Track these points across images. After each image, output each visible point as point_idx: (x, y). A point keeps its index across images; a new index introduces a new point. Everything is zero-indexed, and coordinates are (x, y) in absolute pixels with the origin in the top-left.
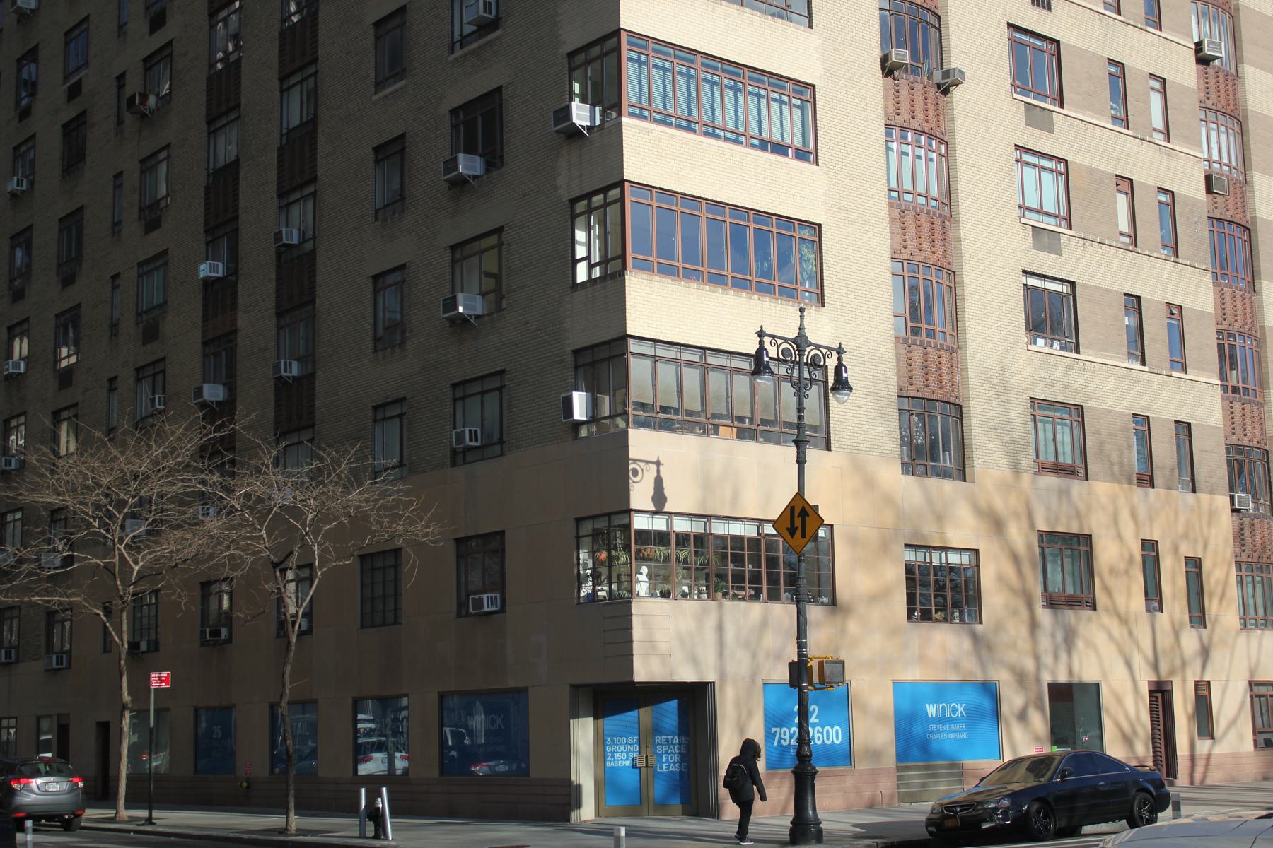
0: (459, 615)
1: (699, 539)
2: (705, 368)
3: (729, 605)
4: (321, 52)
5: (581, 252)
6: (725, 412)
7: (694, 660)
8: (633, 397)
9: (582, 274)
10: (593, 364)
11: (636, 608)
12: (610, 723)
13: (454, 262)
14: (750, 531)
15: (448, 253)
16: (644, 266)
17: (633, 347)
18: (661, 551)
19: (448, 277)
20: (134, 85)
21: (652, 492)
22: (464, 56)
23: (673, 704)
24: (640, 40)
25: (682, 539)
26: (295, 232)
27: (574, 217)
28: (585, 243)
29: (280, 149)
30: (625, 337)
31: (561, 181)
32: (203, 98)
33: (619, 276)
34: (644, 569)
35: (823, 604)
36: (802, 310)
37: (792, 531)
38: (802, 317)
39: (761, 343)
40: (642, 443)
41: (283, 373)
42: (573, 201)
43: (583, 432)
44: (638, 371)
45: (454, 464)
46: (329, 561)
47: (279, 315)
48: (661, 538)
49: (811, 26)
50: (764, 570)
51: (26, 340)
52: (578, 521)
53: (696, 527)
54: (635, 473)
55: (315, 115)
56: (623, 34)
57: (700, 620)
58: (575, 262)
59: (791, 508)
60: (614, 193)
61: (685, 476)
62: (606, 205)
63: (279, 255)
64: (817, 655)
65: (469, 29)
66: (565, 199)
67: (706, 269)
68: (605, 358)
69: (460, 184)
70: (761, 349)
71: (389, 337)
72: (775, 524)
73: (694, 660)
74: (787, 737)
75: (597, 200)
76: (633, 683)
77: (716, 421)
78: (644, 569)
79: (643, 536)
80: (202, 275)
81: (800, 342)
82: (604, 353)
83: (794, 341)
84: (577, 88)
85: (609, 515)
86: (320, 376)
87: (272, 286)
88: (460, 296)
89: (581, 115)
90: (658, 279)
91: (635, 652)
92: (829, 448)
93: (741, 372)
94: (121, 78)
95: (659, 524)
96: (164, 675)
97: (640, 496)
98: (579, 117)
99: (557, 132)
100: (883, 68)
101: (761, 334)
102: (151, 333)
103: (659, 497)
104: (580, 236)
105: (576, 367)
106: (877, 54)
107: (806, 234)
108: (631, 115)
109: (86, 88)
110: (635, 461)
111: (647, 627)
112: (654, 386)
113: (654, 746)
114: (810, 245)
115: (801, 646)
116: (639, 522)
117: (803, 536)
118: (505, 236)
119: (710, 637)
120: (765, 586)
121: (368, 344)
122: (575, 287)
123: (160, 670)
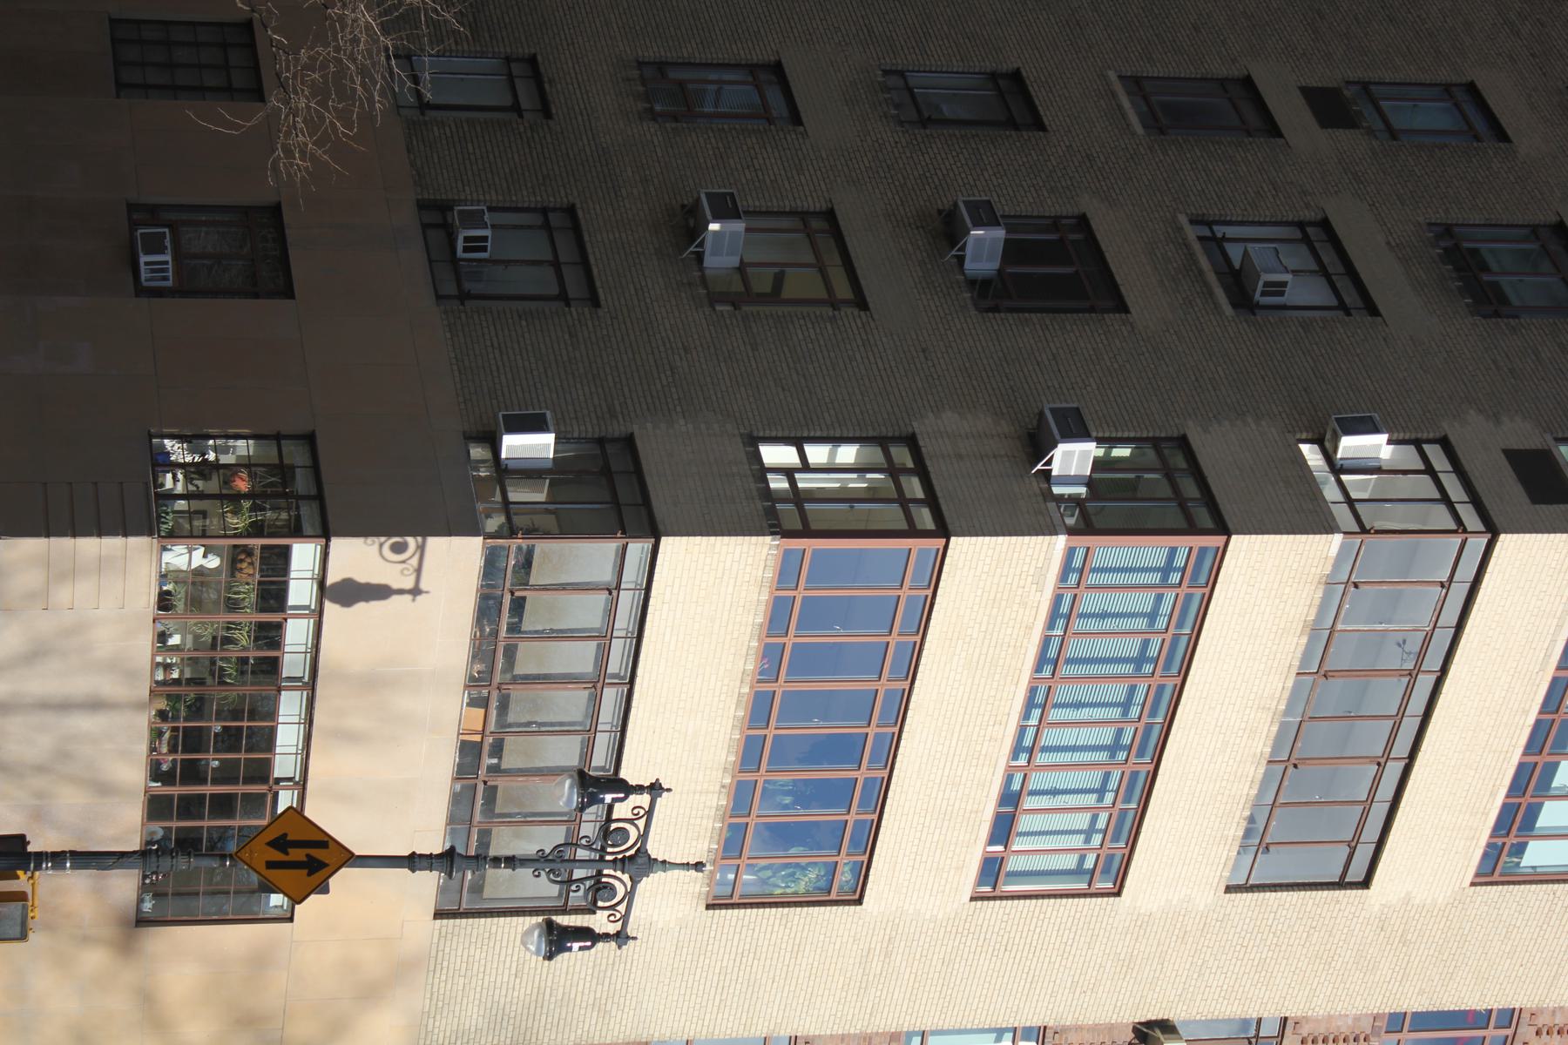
0: (132, 207)
1: (271, 667)
2: (596, 682)
3: (142, 722)
5: (817, 454)
9: (776, 455)
11: (139, 544)
13: (803, 215)
14: (284, 765)
15: (815, 204)
16: (787, 572)
17: (638, 549)
18: (247, 590)
21: (362, 578)
22: (1187, 246)
24: (1209, 573)
25: (270, 635)
27: (883, 442)
28: (834, 461)
34: (213, 562)
35: (140, 901)
36: (698, 866)
37: (281, 843)
38: (686, 866)
39: (639, 789)
40: (455, 563)
42: (911, 442)
43: (478, 452)
44: (592, 557)
48: (274, 595)
49: (1229, 889)
50: (208, 789)
52: (310, 439)
53: (293, 662)
54: (399, 549)
57: (116, 666)
58: (798, 443)
59: (324, 841)
60: (925, 518)
61: (391, 646)
62: (904, 502)
66: (917, 427)
69: (949, 231)
70: (628, 789)
72: (297, 812)
75: (914, 487)
77: (494, 704)
79: (279, 561)
81: (640, 863)
82: (626, 492)
84: (1122, 452)
85: (319, 497)
89: (1072, 459)
90: (765, 597)
91: (53, 539)
92: (439, 915)
95: (300, 592)
97: (355, 557)
98: (1067, 454)
99: (1041, 414)
100: (1150, 1024)
101: (655, 789)
103: (352, 593)
104: (848, 454)
105: (601, 442)
106: (1175, 1014)
107: (844, 876)
108: (1070, 553)
110: (421, 549)
111: (101, 565)
112: (563, 587)
115: (57, 858)
116: (303, 555)
117: (271, 865)
119: (82, 685)
120: (176, 790)
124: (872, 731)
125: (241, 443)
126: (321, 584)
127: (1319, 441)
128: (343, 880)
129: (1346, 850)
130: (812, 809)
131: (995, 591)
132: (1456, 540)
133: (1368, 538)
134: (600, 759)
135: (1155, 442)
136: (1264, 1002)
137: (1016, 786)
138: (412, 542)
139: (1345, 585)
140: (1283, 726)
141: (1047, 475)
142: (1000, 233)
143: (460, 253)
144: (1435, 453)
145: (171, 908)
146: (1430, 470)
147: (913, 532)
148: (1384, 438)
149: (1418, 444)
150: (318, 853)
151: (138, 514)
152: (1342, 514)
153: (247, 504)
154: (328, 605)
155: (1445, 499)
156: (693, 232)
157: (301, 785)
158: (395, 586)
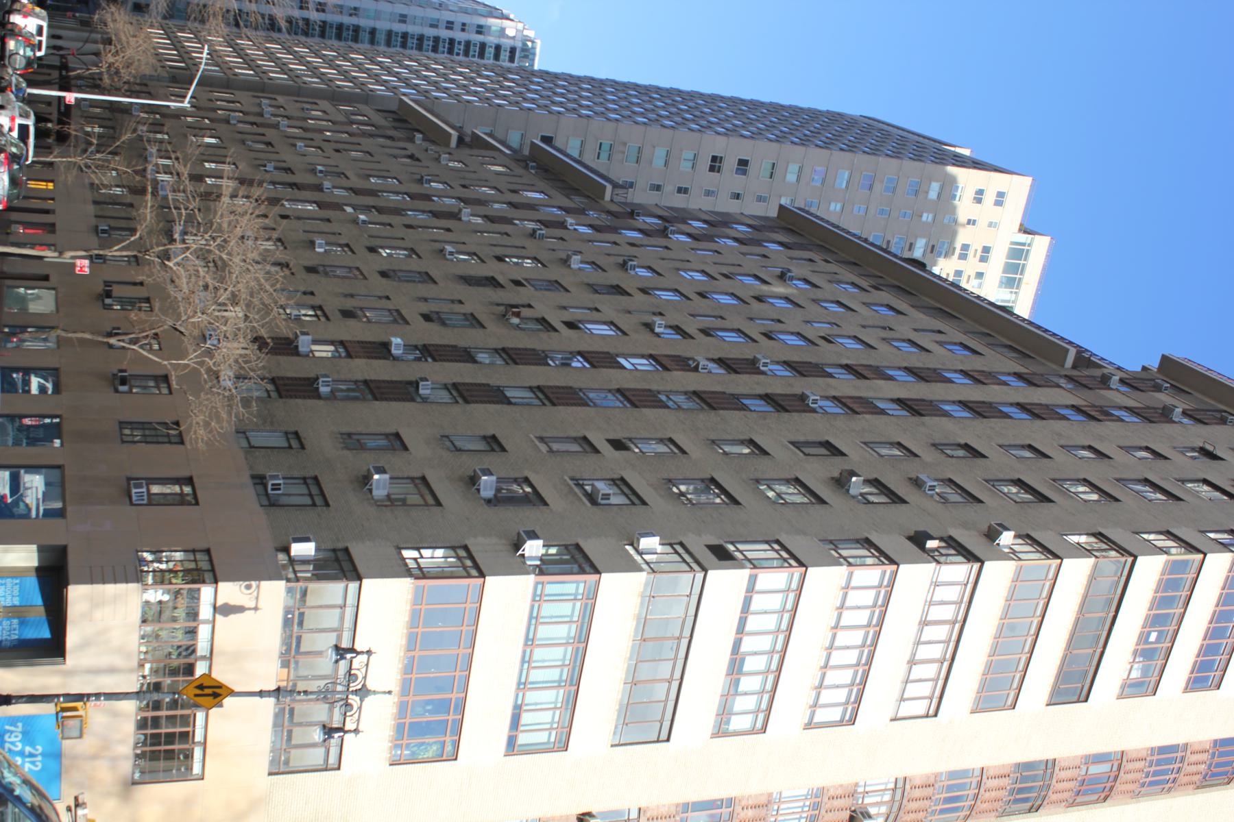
1: (191, 650)
4: (560, 408)
5: (426, 553)
6: (294, 742)
7: (85, 645)
8: (313, 586)
9: (407, 554)
10: (337, 560)
11: (133, 587)
12: (32, 583)
13: (412, 479)
15: (419, 475)
16: (418, 598)
17: (353, 586)
18: (181, 613)
19: (400, 475)
20: (525, 312)
21: (232, 602)
23: (46, 633)
24: (591, 598)
26: (428, 392)
27: (453, 548)
28: (434, 557)
29: (488, 385)
30: (360, 578)
31: (480, 539)
32: (521, 346)
33: (408, 573)
34: (166, 598)
35: (133, 773)
36: (390, 692)
37: (201, 687)
38: (384, 693)
39: (362, 652)
40: (274, 593)
41: (321, 379)
42: (466, 548)
43: (282, 557)
44: (332, 590)
45: (253, 477)
46: (175, 370)
47: (366, 382)
48: (193, 614)
50: (163, 713)
51: (330, 355)
52: (208, 551)
53: (202, 647)
54: (248, 587)
55: (515, 404)
56: (596, 576)
58: (418, 549)
59: (220, 686)
61: (246, 626)
62: (465, 567)
63: (410, 383)
64: (90, 714)
65: (588, 488)
66: (467, 542)
67: (414, 676)
68: (340, 565)
69: (473, 480)
70: (358, 653)
71: (352, 441)
72: (208, 676)
73: (85, 645)
74: (13, 739)
76: (66, 584)
77: (292, 666)
78: (166, 598)
79: (195, 597)
80: (393, 339)
81: (363, 692)
82: (346, 566)
83: (364, 685)
84: (553, 551)
86: (321, 402)
87: (387, 378)
88: (387, 476)
90: (408, 608)
91: (95, 586)
92: (270, 774)
93: (339, 638)
94: (530, 306)
95: (205, 612)
96: (87, 270)
97: (230, 591)
98: (531, 546)
99: (519, 534)
100: (583, 814)
101: (369, 652)
102: (347, 314)
104: (440, 553)
105: (334, 550)
107: (449, 748)
109: (520, 289)
110: (258, 587)
111: (116, 598)
112: (321, 607)
113: (9, 618)
114: (439, 752)
117: (196, 695)
118: (436, 509)
119: (105, 660)
121: (345, 429)
122: (399, 549)
123: (90, 267)
124: (458, 674)
125: (178, 554)
126: (215, 607)
127: (632, 544)
128: (228, 701)
129: (658, 725)
130: (431, 728)
131: (506, 597)
132: (691, 575)
133: (658, 575)
134: (345, 644)
135: (566, 546)
136: (628, 802)
137: (519, 702)
138: (254, 584)
139: (650, 597)
140: (629, 665)
141: (523, 555)
142: (494, 478)
143: (270, 491)
144: (678, 548)
145: (147, 777)
146: (676, 552)
147: (469, 576)
148: (657, 539)
149: (671, 545)
150: (217, 690)
151: (132, 573)
152: (645, 566)
153: (181, 574)
154: (218, 616)
155: (684, 561)
156: (367, 479)
157: (210, 658)
158: (247, 606)
